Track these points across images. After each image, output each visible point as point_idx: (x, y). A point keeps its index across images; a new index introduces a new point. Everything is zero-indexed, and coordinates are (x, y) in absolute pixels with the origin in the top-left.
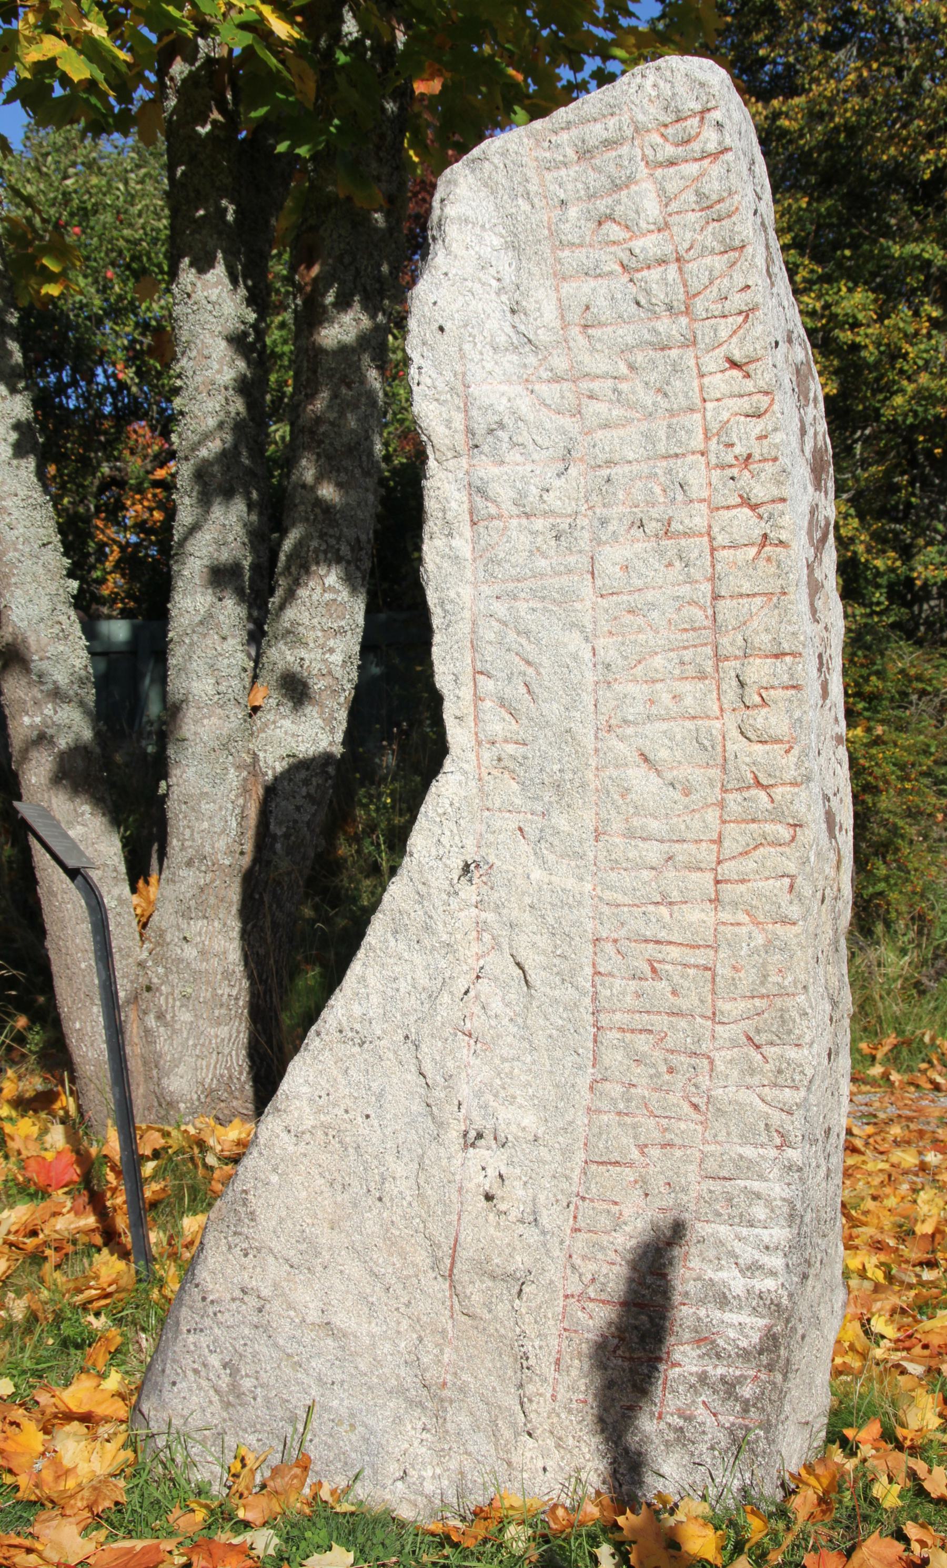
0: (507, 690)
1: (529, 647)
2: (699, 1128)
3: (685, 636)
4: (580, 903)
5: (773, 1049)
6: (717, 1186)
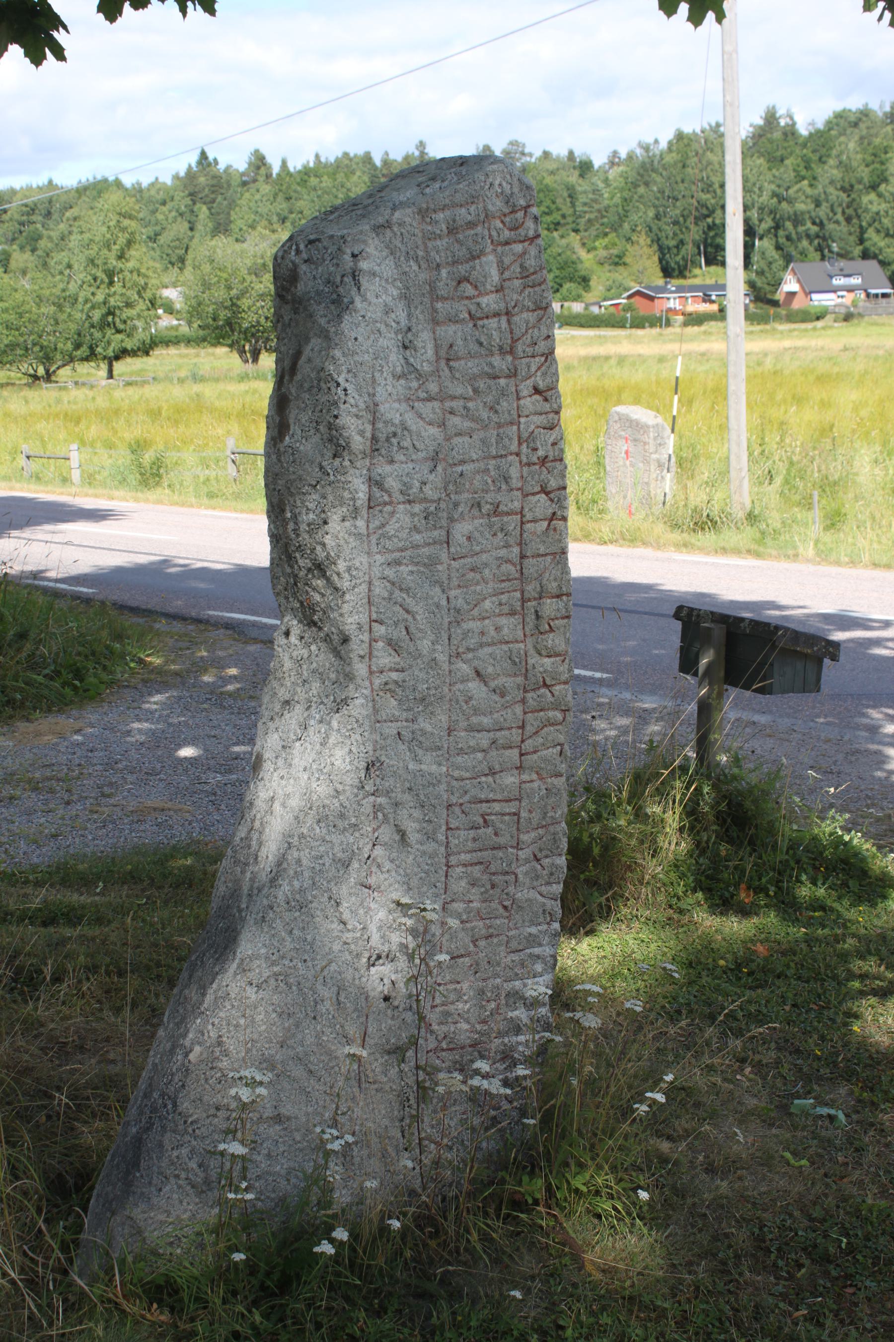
0: (395, 634)
1: (409, 600)
2: (506, 921)
3: (503, 585)
4: (439, 781)
5: (547, 860)
6: (515, 957)
